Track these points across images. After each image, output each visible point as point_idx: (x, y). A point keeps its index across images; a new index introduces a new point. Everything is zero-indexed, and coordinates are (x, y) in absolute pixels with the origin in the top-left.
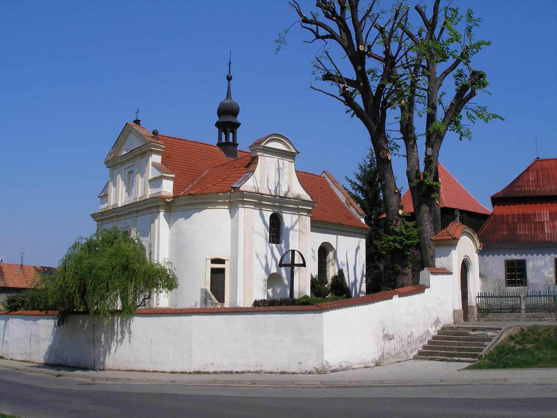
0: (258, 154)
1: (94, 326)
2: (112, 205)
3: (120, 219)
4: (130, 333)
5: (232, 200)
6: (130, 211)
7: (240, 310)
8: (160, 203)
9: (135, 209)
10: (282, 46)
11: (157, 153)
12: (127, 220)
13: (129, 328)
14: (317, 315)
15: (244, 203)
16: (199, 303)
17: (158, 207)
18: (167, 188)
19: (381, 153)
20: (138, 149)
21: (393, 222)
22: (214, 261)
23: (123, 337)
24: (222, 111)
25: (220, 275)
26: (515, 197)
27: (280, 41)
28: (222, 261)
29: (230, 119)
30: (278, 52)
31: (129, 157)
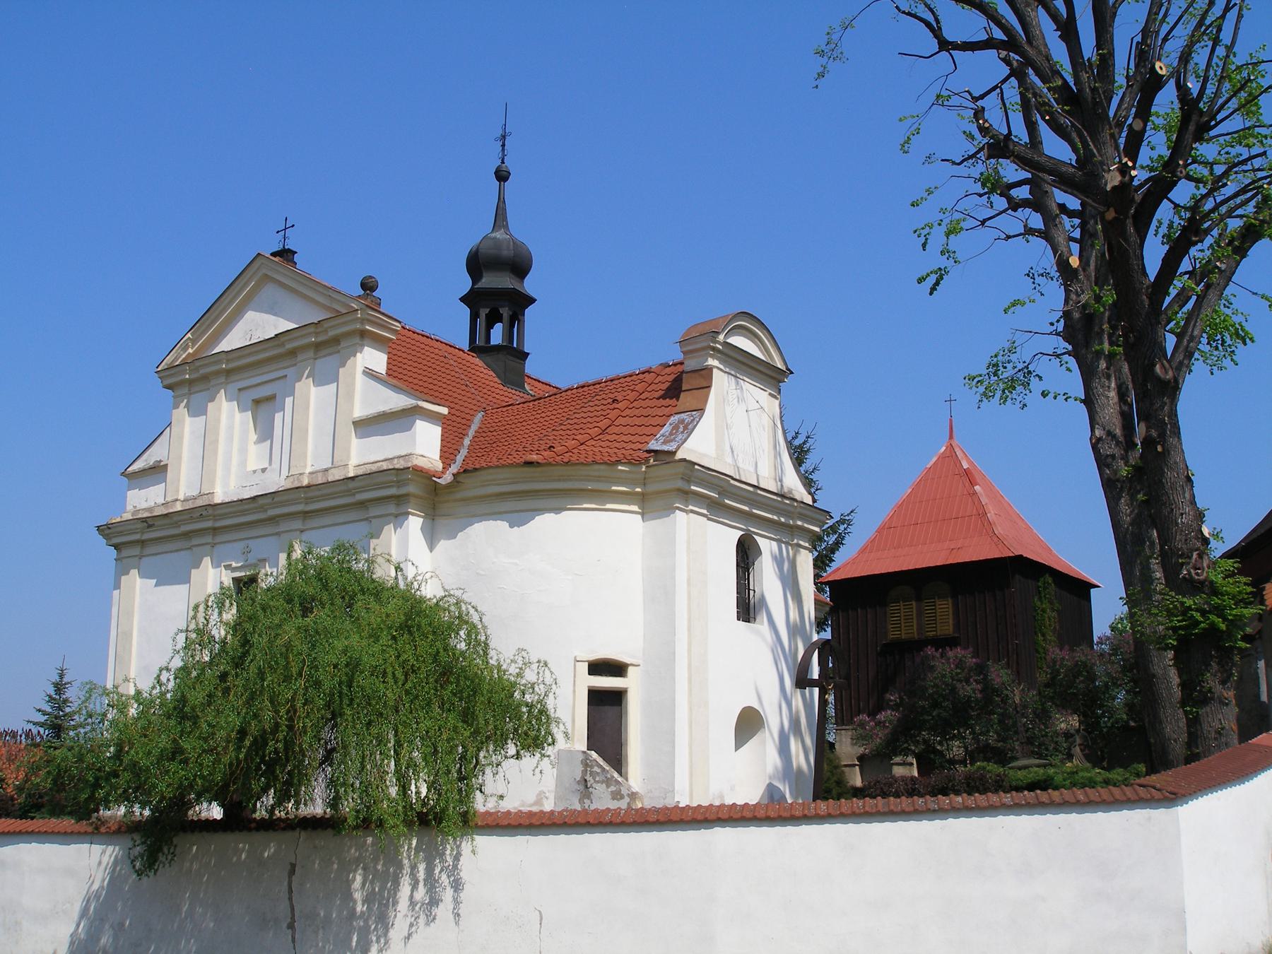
0: (712, 362)
1: (292, 872)
2: (181, 497)
3: (218, 539)
4: (457, 885)
5: (651, 488)
6: (271, 513)
7: (748, 814)
8: (411, 489)
9: (300, 507)
10: (832, 66)
11: (379, 342)
12: (250, 542)
13: (455, 867)
14: (1159, 815)
15: (687, 496)
16: (552, 796)
17: (400, 500)
18: (424, 443)
19: (1158, 368)
20: (312, 329)
21: (1190, 558)
22: (598, 668)
23: (434, 901)
24: (476, 264)
25: (609, 711)
27: (829, 51)
28: (618, 669)
29: (502, 281)
30: (821, 82)
31: (267, 354)
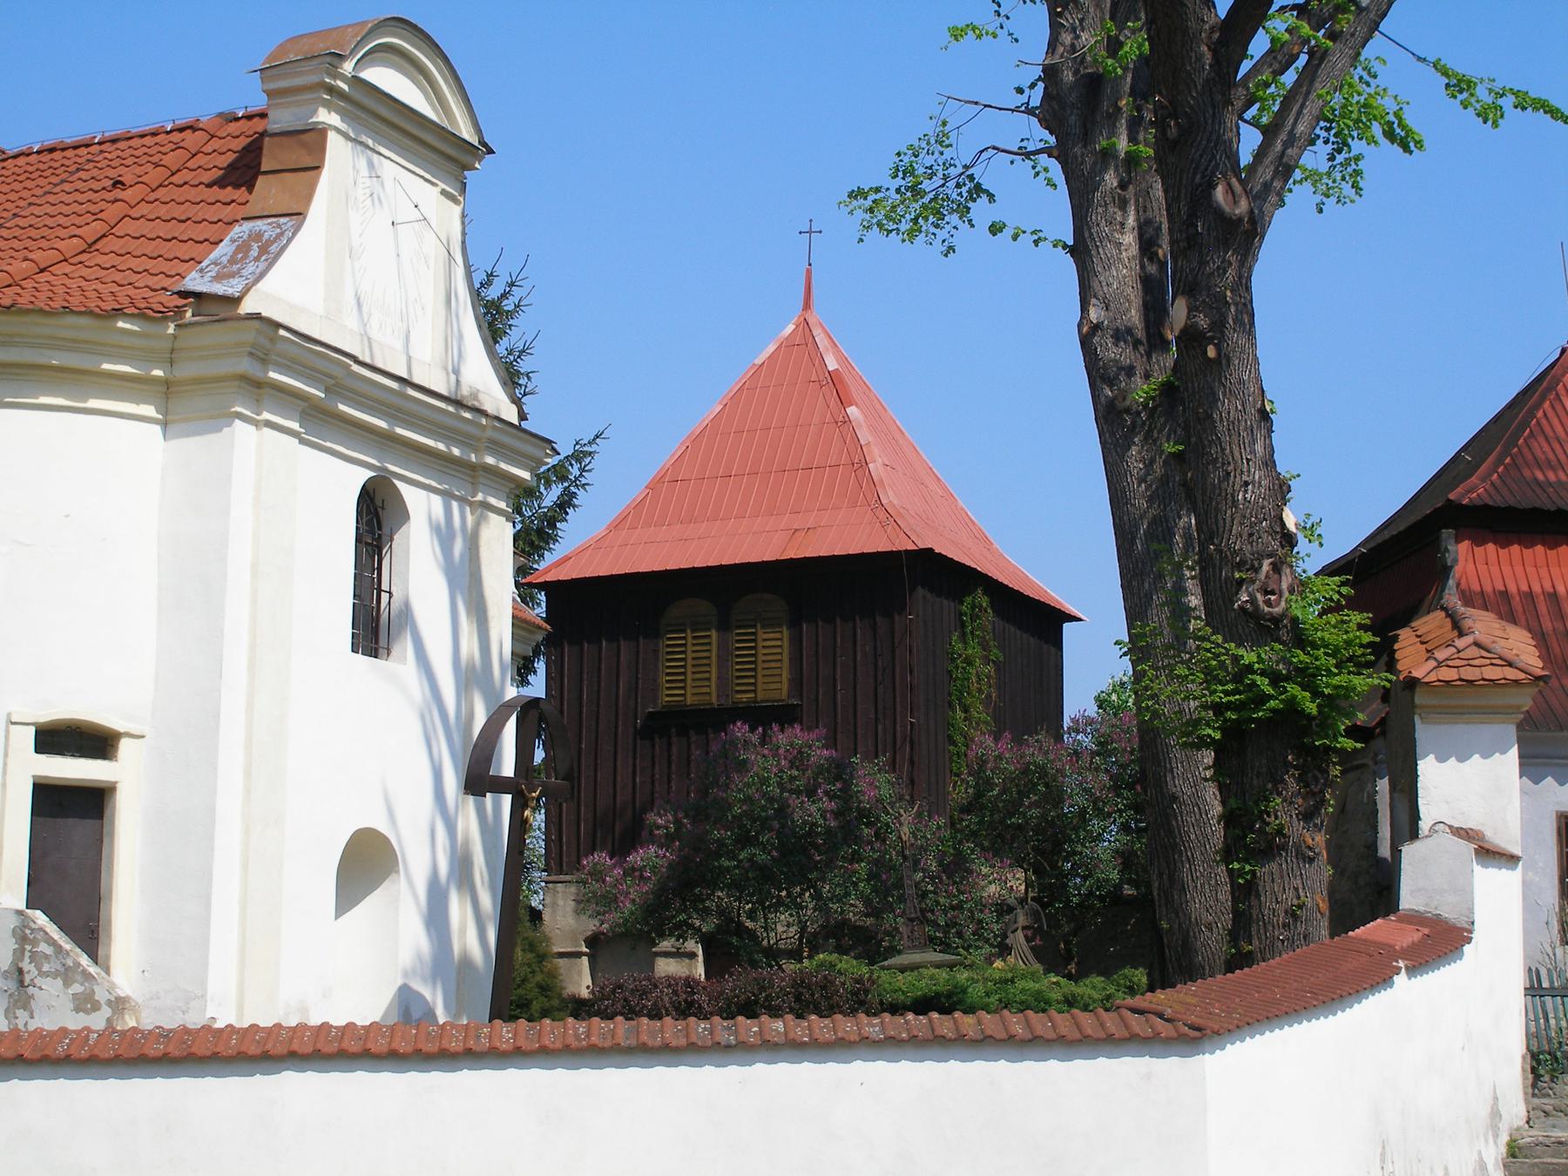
5: (185, 371)
15: (258, 390)
21: (1257, 570)
22: (52, 738)
25: (76, 829)
26: (1535, 511)
28: (93, 741)
